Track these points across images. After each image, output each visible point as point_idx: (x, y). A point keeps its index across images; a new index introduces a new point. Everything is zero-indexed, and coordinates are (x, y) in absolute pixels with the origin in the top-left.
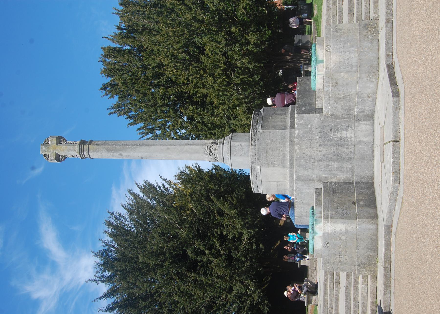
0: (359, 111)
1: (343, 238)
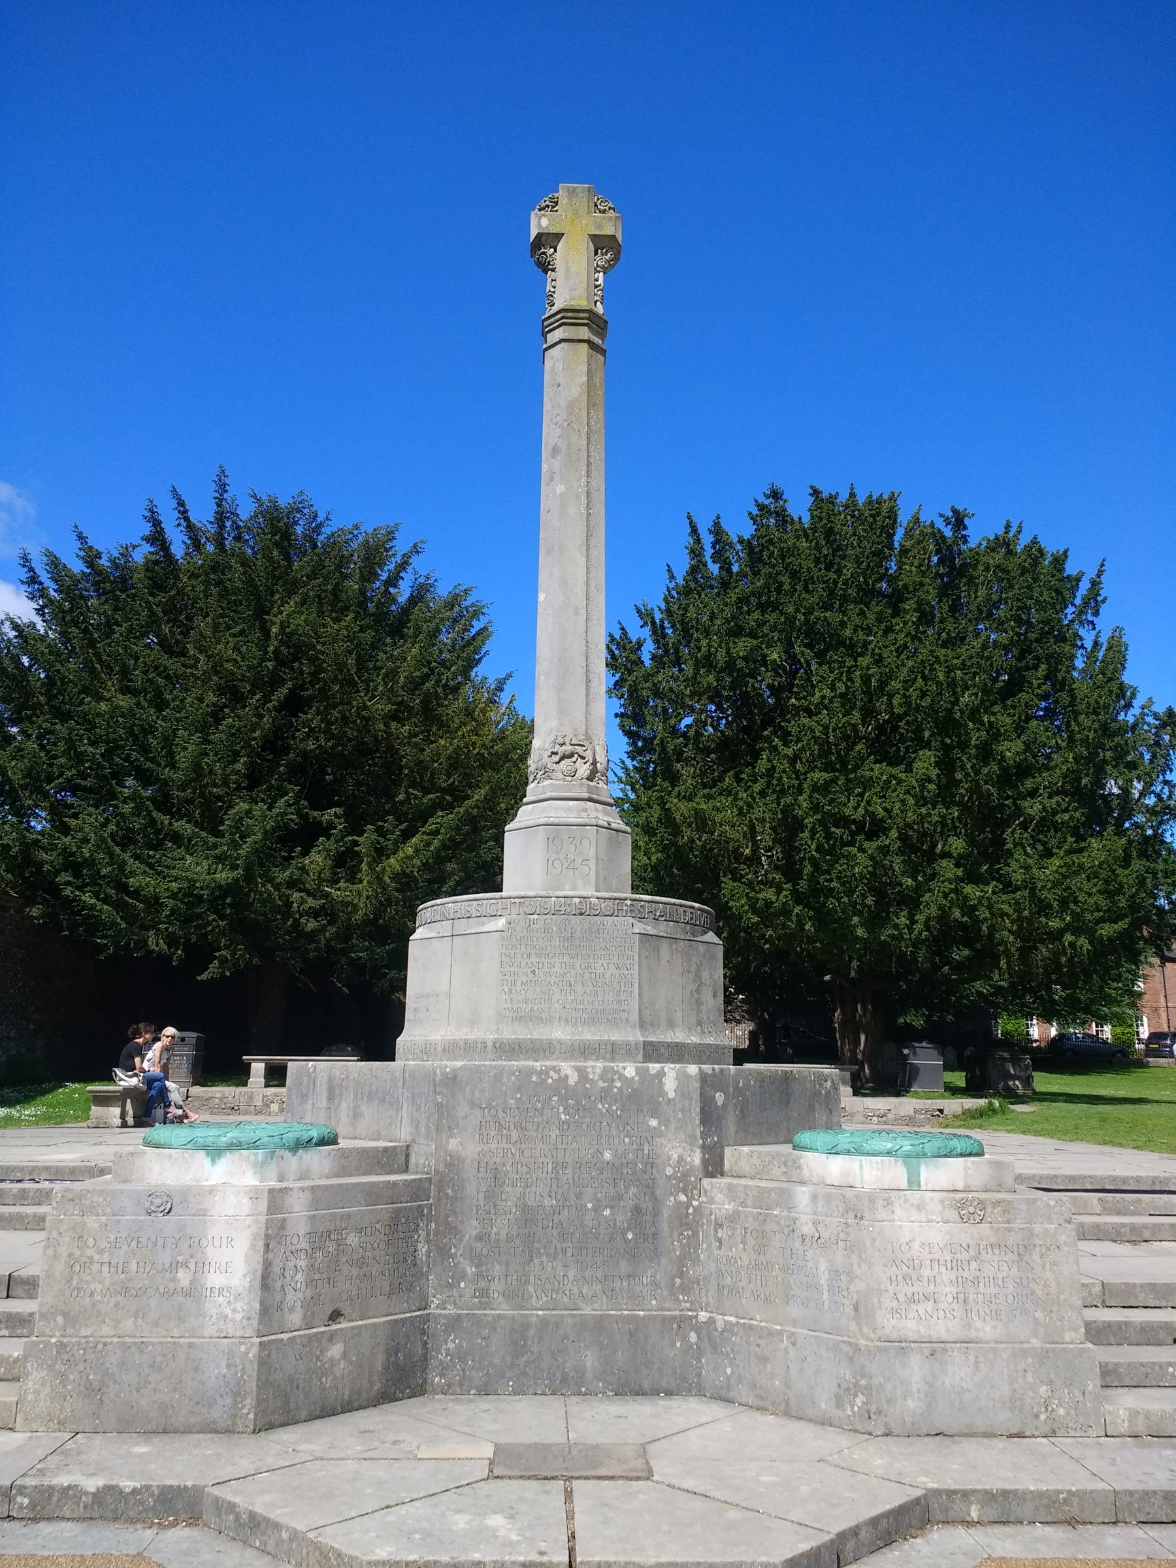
0: (716, 1330)
1: (184, 1278)
